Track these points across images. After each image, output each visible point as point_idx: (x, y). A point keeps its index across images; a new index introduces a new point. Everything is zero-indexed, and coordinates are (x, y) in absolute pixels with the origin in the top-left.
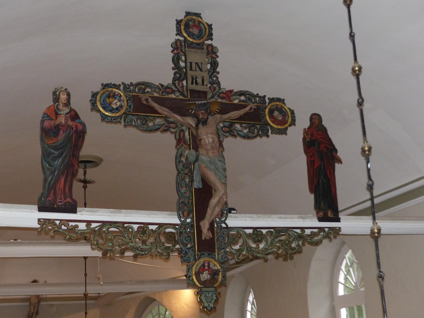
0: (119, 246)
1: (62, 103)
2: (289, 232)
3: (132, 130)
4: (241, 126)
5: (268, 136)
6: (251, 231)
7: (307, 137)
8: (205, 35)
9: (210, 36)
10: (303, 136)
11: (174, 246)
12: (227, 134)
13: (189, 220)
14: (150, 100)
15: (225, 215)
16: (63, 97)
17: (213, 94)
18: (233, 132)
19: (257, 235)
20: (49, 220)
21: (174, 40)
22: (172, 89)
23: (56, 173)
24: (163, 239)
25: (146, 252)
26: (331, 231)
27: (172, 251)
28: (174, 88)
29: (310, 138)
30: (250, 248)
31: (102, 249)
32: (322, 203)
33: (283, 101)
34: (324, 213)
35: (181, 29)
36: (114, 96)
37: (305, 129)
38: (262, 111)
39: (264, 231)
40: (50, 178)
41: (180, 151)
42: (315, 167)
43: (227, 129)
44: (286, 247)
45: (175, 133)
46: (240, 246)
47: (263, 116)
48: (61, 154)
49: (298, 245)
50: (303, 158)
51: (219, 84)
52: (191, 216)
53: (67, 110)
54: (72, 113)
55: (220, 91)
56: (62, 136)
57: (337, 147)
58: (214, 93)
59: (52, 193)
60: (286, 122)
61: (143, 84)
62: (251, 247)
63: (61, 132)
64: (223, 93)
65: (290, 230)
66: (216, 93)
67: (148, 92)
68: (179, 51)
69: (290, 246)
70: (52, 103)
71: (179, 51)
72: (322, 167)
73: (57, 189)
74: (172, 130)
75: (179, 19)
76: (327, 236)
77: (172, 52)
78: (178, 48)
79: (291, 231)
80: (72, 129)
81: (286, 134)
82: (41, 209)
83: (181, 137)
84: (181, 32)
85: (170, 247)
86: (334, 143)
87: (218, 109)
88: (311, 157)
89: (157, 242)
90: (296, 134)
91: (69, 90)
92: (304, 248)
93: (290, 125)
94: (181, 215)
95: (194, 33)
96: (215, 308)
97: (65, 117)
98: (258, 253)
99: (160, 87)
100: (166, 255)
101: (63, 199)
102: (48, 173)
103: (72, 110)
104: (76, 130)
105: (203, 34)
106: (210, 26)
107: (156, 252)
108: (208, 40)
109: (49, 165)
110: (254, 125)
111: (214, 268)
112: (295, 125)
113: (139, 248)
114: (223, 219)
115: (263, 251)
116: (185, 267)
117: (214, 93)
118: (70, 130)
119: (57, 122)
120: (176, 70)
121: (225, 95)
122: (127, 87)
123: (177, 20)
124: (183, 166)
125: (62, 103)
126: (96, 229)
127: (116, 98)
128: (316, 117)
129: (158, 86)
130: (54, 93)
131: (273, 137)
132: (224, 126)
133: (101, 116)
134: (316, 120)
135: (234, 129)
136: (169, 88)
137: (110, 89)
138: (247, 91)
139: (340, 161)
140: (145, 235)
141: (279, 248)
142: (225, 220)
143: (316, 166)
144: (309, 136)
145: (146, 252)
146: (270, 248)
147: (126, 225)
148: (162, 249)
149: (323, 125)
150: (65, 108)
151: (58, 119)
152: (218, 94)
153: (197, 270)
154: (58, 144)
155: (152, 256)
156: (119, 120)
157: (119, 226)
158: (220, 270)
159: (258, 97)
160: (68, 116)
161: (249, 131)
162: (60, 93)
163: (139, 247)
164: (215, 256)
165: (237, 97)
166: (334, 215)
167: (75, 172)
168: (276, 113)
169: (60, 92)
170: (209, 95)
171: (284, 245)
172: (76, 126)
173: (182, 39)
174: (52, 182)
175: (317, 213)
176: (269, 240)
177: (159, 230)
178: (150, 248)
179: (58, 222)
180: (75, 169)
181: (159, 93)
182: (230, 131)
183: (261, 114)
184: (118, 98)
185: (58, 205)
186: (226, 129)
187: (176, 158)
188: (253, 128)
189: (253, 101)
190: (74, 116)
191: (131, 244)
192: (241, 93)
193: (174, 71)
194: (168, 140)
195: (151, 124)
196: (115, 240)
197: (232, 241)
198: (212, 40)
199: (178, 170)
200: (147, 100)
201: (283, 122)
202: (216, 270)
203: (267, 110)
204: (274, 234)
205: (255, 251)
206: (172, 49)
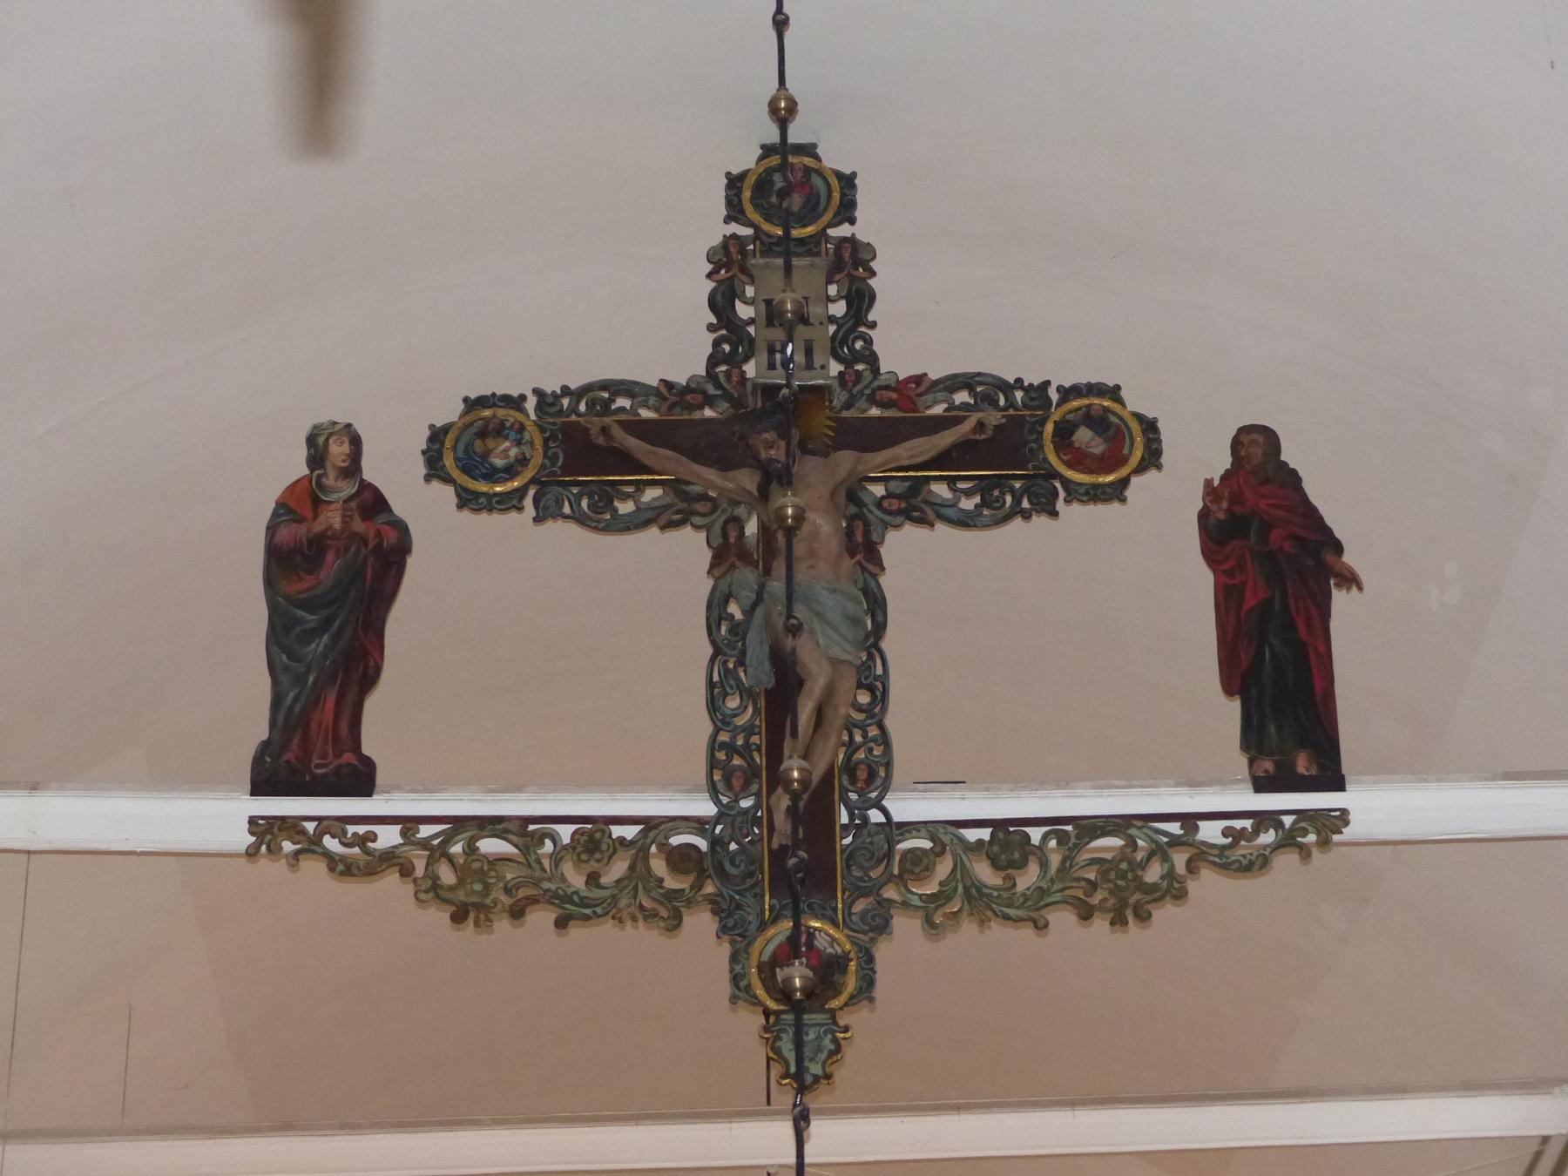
0: (508, 891)
1: (335, 467)
2: (1133, 831)
3: (563, 532)
4: (953, 489)
5: (1054, 514)
6: (985, 834)
7: (1214, 507)
8: (825, 210)
9: (847, 211)
10: (1200, 505)
11: (697, 886)
12: (899, 519)
13: (746, 803)
14: (618, 433)
15: (879, 782)
16: (338, 451)
17: (852, 396)
18: (921, 510)
19: (1006, 846)
20: (283, 818)
21: (717, 240)
22: (704, 393)
23: (311, 679)
24: (659, 866)
25: (599, 910)
26: (1303, 824)
27: (690, 903)
28: (711, 390)
29: (1229, 511)
30: (979, 890)
31: (453, 903)
32: (1272, 729)
33: (1114, 393)
34: (1278, 765)
35: (740, 200)
36: (500, 431)
37: (1208, 483)
38: (1031, 432)
39: (1036, 834)
40: (292, 694)
41: (723, 586)
42: (1246, 607)
43: (895, 504)
44: (1121, 883)
45: (708, 528)
46: (941, 884)
47: (1031, 451)
48: (325, 625)
49: (1170, 875)
50: (1202, 581)
51: (872, 359)
52: (755, 788)
53: (349, 489)
54: (366, 495)
55: (876, 384)
56: (332, 567)
57: (1339, 534)
58: (855, 391)
59: (296, 741)
60: (1123, 461)
61: (604, 385)
62: (980, 887)
63: (330, 556)
64: (887, 388)
65: (1139, 823)
66: (861, 392)
67: (622, 409)
68: (735, 270)
69: (1137, 878)
70: (307, 472)
71: (735, 270)
72: (1277, 607)
73: (314, 726)
74: (697, 520)
75: (735, 172)
76: (1288, 841)
77: (709, 276)
78: (729, 266)
79: (1139, 828)
80: (366, 545)
81: (1123, 500)
82: (260, 788)
83: (732, 541)
84: (742, 211)
85: (683, 890)
86: (1328, 521)
87: (830, 428)
88: (1230, 573)
89: (639, 873)
90: (1163, 513)
91: (360, 428)
92: (1192, 886)
93: (1140, 469)
94: (720, 786)
95: (790, 211)
96: (828, 1077)
97: (344, 510)
98: (1009, 906)
99: (663, 390)
100: (669, 913)
101: (331, 757)
102: (285, 679)
103: (366, 487)
104: (378, 548)
105: (822, 207)
106: (848, 182)
107: (633, 909)
108: (841, 223)
109: (290, 657)
110: (1000, 482)
111: (830, 950)
112: (1159, 467)
113: (575, 898)
114: (874, 795)
115: (1026, 900)
116: (725, 950)
117: (855, 391)
118: (358, 548)
119: (318, 528)
120: (724, 332)
121: (894, 396)
122: (550, 400)
123: (728, 174)
124: (731, 631)
125: (335, 467)
126: (436, 842)
127: (506, 438)
128: (1256, 436)
129: (657, 389)
130: (311, 440)
131: (1072, 513)
132: (889, 495)
133: (458, 495)
134: (1256, 450)
135: (926, 502)
136: (693, 391)
137: (487, 413)
138: (979, 374)
139: (1350, 580)
140: (598, 856)
141: (1093, 886)
142: (881, 797)
143: (1250, 603)
144: (1225, 505)
145: (599, 910)
146: (1056, 887)
147: (532, 827)
148: (654, 900)
149: (1285, 464)
150: (340, 484)
151: (321, 518)
152: (868, 392)
153: (765, 958)
154: (317, 592)
155: (621, 921)
156: (515, 502)
157: (507, 831)
158: (852, 955)
159: (1022, 388)
160: (353, 505)
161: (984, 503)
162: (327, 440)
163: (576, 893)
164: (835, 910)
165: (940, 396)
166: (1321, 767)
167: (371, 672)
168: (1083, 435)
169: (330, 435)
170: (840, 397)
171: (1112, 875)
172: (379, 534)
173: (747, 231)
174: (297, 708)
175: (1251, 762)
176: (1055, 860)
177: (646, 837)
178: (614, 897)
179: (310, 827)
180: (372, 663)
181: (657, 410)
182: (914, 507)
183: (1027, 442)
184: (512, 435)
185: (314, 776)
186: (894, 501)
187: (709, 607)
188: (996, 493)
189: (1002, 402)
190: (373, 503)
191: (546, 885)
192: (954, 383)
193: (714, 335)
194: (684, 554)
195: (625, 508)
196: (493, 874)
197: (908, 866)
198: (852, 221)
199: (713, 642)
200: (605, 430)
201: (1113, 460)
202: (836, 956)
203: (1049, 428)
204: (1073, 840)
205: (999, 896)
206: (709, 267)
